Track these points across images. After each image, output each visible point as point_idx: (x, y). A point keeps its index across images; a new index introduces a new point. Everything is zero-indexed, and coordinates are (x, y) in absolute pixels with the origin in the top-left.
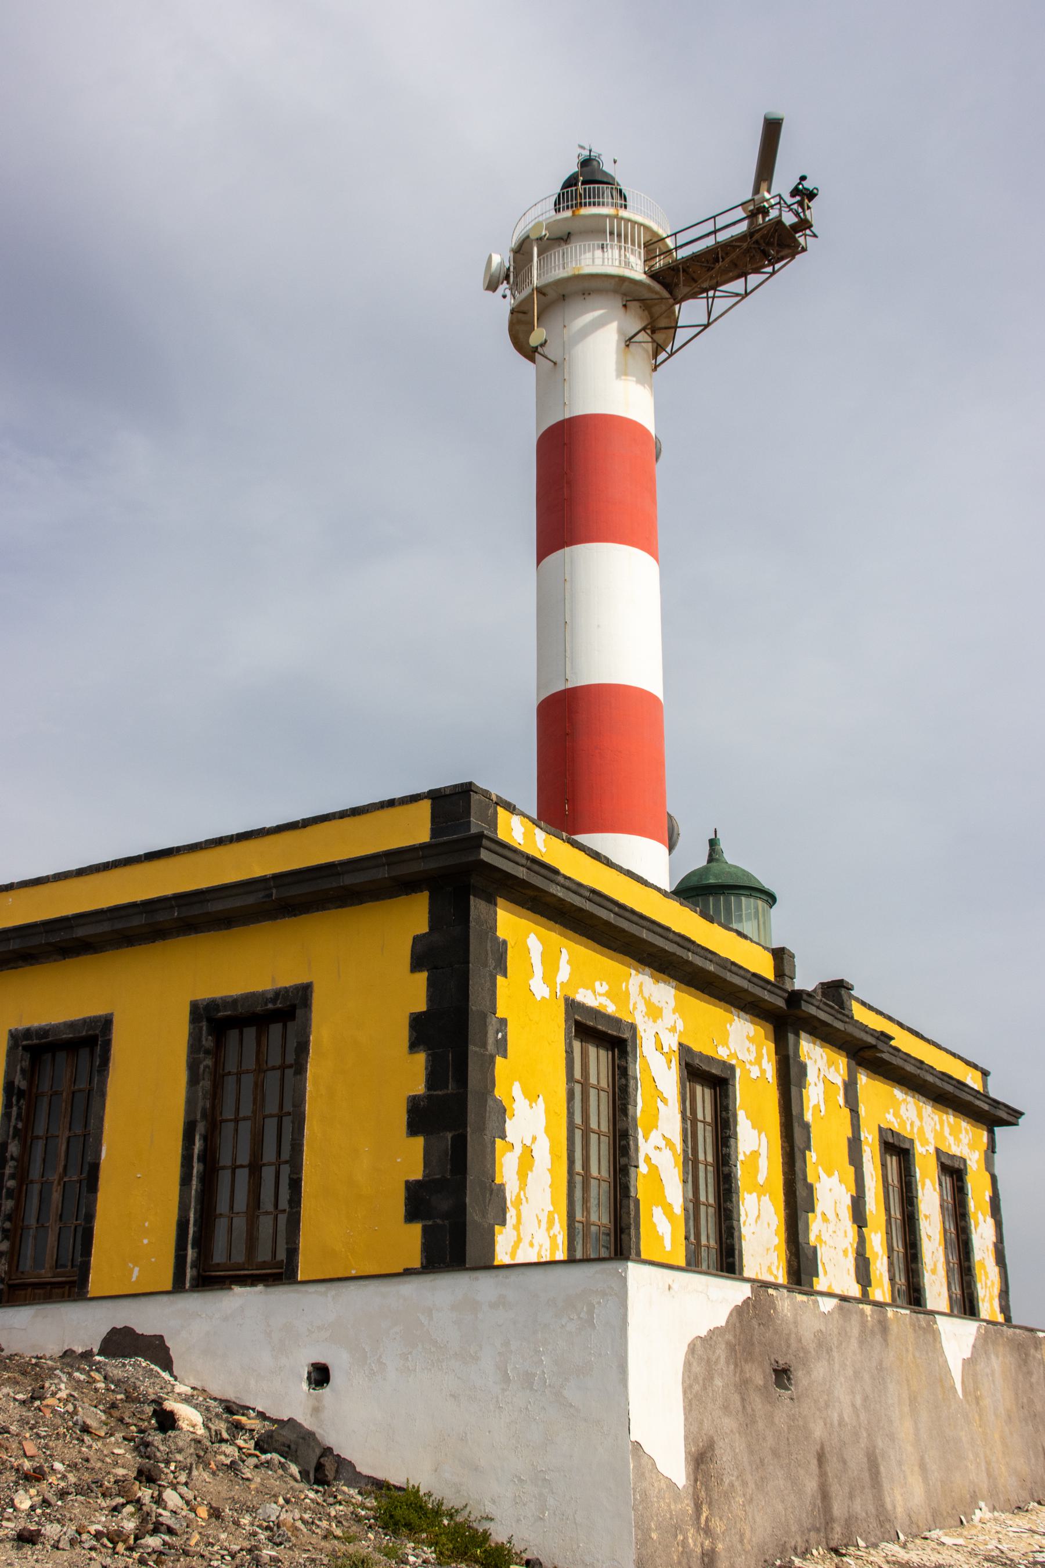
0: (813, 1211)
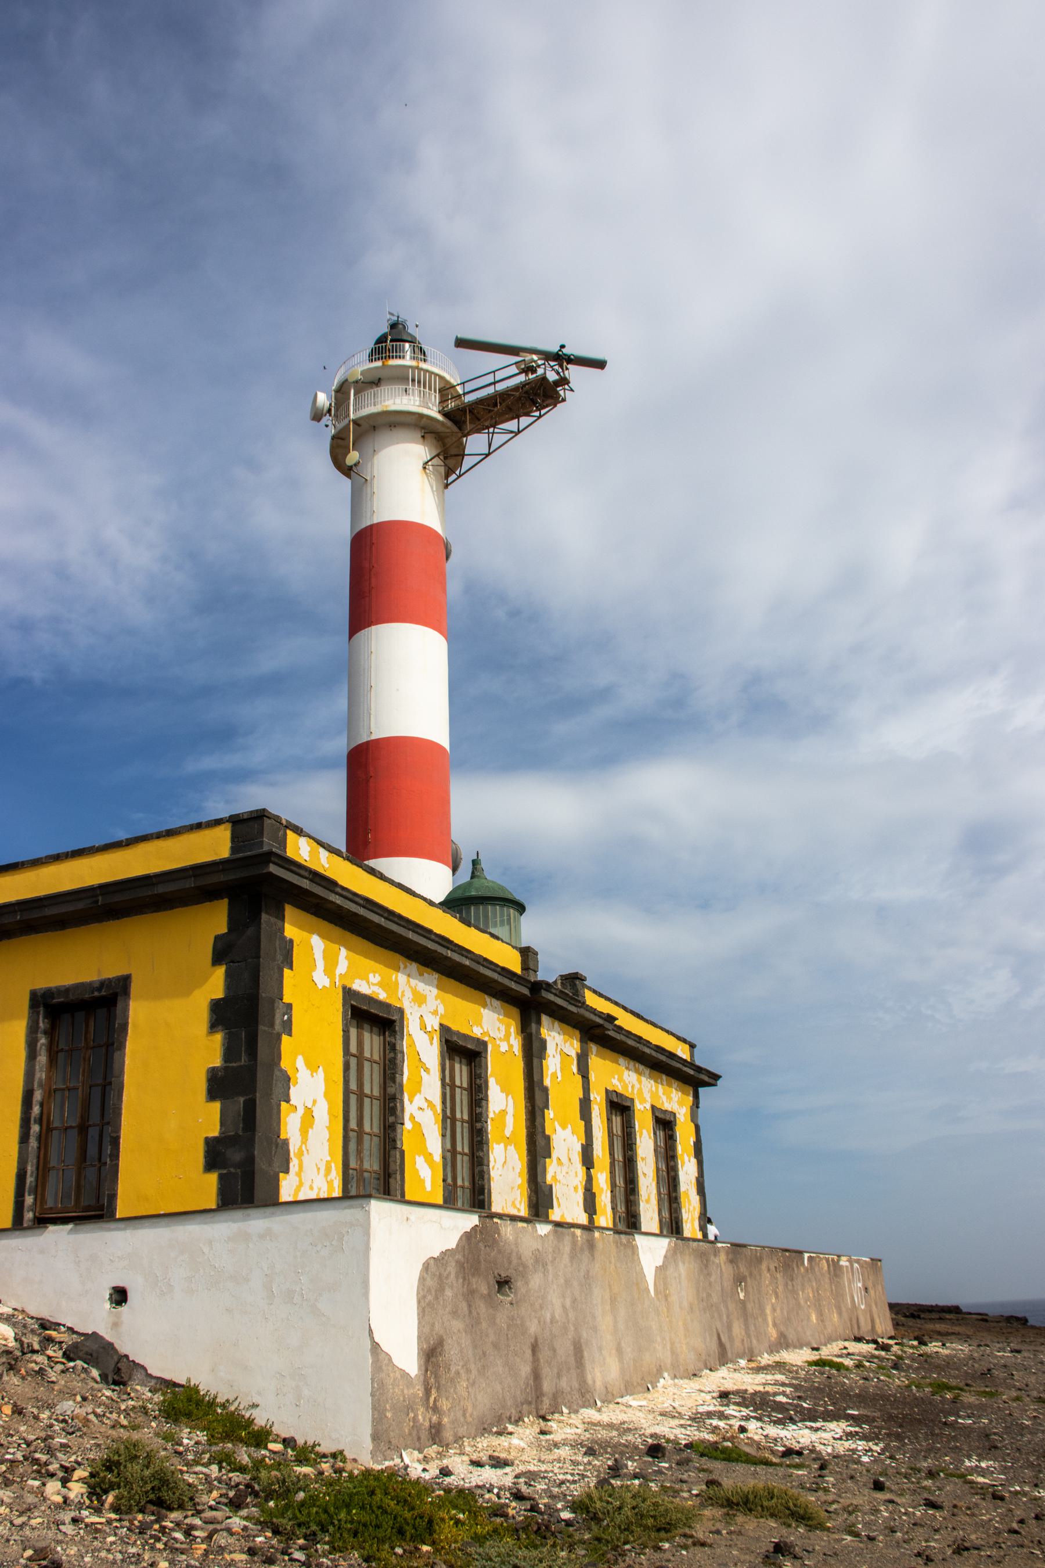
0: (550, 1156)
